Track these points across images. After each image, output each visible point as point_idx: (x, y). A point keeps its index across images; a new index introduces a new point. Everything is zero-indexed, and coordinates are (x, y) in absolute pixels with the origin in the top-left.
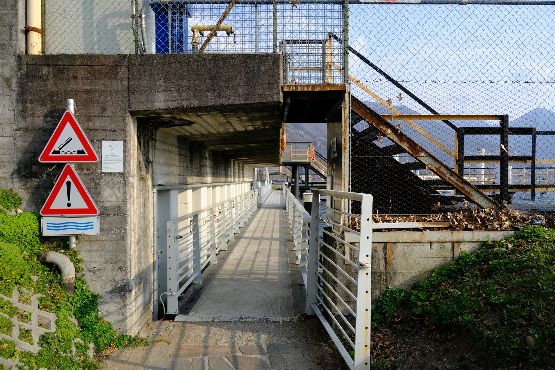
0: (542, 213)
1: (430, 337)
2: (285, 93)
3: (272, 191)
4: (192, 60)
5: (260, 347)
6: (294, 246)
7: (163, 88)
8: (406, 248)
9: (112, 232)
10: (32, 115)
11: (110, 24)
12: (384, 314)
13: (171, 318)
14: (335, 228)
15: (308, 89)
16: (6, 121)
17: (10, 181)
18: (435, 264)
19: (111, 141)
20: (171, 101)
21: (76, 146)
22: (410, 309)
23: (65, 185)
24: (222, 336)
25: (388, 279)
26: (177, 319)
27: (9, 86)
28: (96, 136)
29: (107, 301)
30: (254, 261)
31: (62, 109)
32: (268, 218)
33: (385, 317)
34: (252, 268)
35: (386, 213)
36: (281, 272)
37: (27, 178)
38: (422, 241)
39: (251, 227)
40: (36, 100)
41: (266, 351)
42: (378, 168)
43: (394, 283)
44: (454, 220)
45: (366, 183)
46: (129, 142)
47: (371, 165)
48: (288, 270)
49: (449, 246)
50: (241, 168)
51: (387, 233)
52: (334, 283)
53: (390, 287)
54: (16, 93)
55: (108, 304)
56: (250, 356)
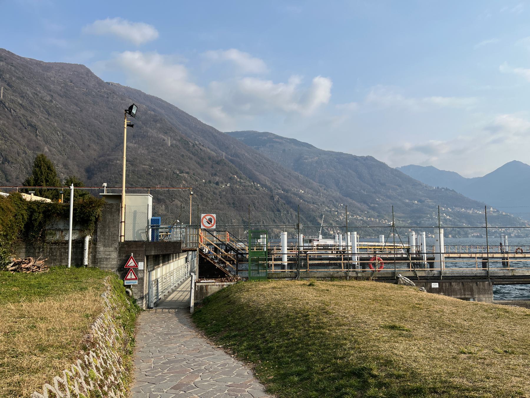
11: (139, 232)
13: (152, 308)
27: (117, 250)
39: (182, 287)
49: (221, 286)
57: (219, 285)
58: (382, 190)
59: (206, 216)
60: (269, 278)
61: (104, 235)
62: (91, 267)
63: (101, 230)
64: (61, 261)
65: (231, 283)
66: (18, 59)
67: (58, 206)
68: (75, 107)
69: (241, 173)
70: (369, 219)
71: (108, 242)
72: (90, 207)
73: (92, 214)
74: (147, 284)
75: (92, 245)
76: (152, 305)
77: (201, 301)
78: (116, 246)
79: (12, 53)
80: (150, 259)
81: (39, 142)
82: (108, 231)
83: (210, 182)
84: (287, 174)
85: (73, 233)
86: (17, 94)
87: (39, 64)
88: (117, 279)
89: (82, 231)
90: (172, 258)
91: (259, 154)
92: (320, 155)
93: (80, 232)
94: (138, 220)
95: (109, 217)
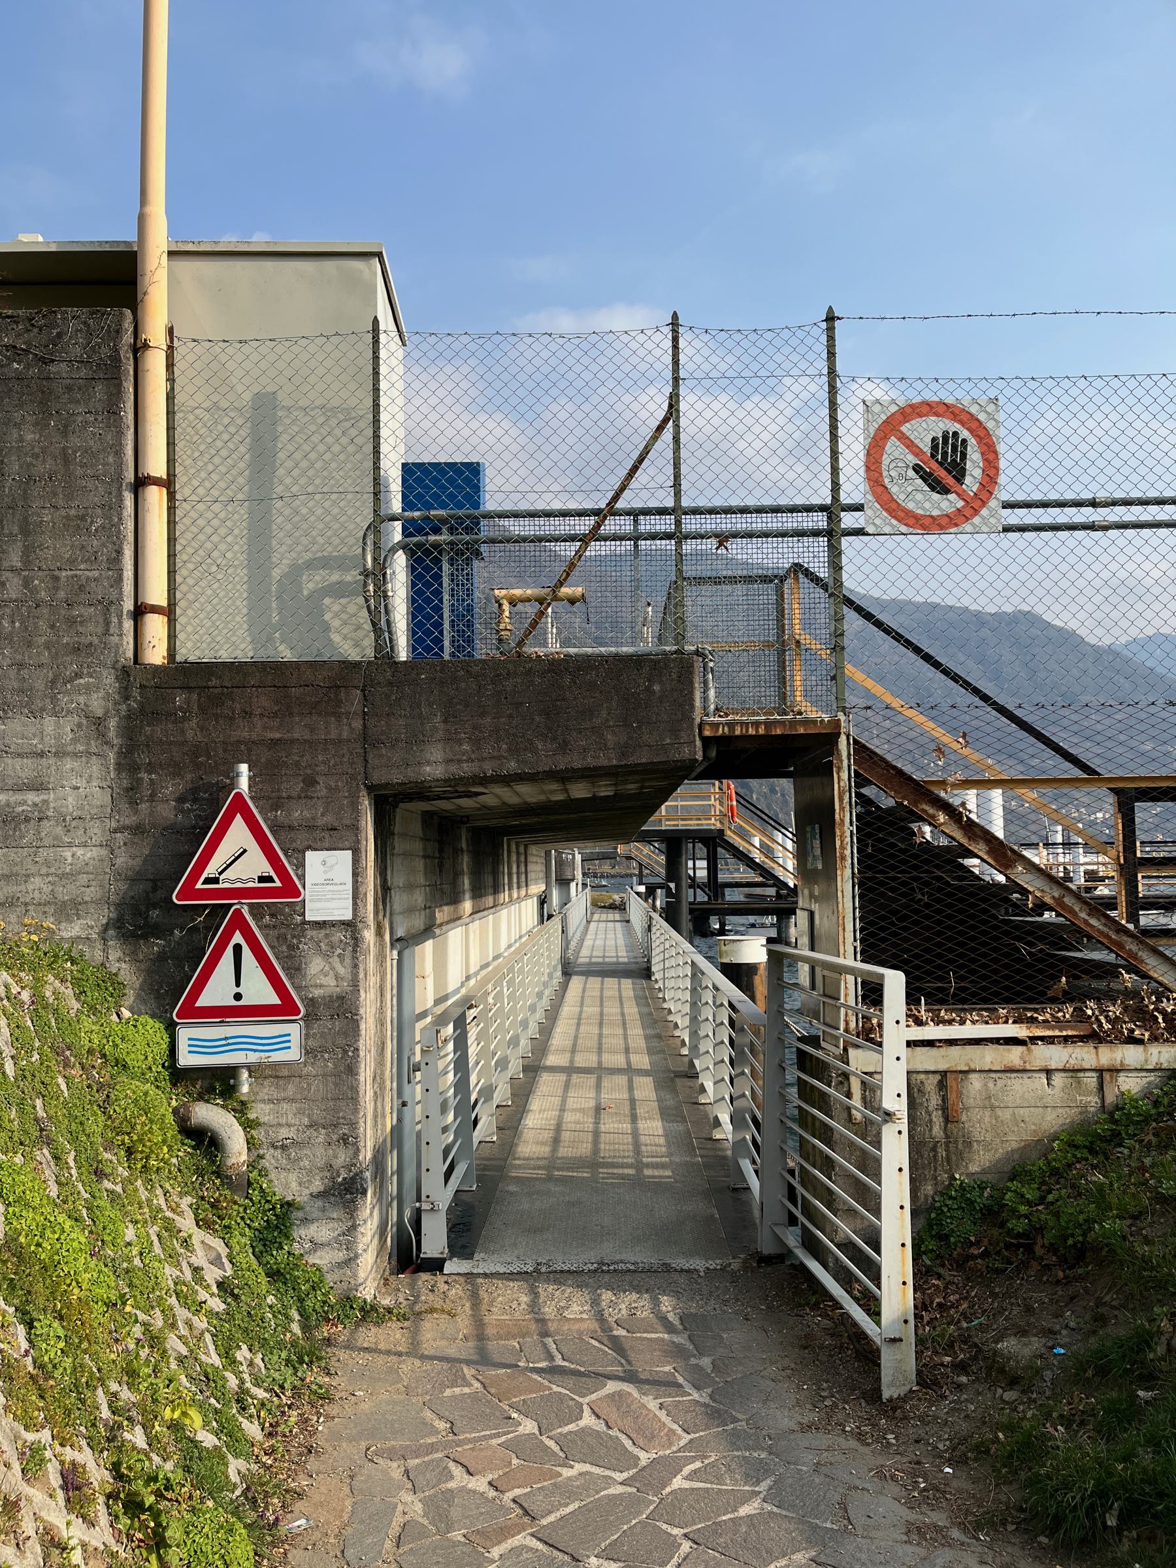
1: (1045, 1279)
2: (706, 741)
3: (592, 914)
4: (504, 673)
5: (663, 1319)
6: (703, 1090)
7: (440, 734)
8: (991, 1085)
9: (326, 1056)
12: (946, 1238)
13: (436, 1266)
14: (828, 1038)
15: (757, 731)
16: (94, 811)
17: (99, 945)
18: (1061, 1121)
19: (325, 852)
20: (460, 761)
21: (254, 866)
22: (1002, 1225)
24: (569, 1299)
25: (954, 1158)
26: (449, 1267)
28: (293, 840)
29: (314, 1216)
31: (217, 783)
32: (602, 1005)
33: (948, 1244)
34: (596, 1150)
35: (941, 1004)
36: (677, 1159)
37: (138, 937)
38: (1028, 1068)
39: (560, 1037)
40: (161, 765)
41: (681, 1327)
42: (921, 900)
43: (967, 1167)
44: (1102, 1018)
45: (894, 934)
46: (364, 853)
47: (904, 895)
48: (696, 1155)
49: (1091, 1080)
50: (522, 858)
51: (955, 1051)
52: (828, 1165)
53: (957, 1176)
54: (116, 749)
55: (316, 1224)
56: (645, 1335)
57: (1074, 1072)
71: (21, 665)
74: (389, 1047)
78: (97, 704)
82: (15, 560)
85: (847, 1236)
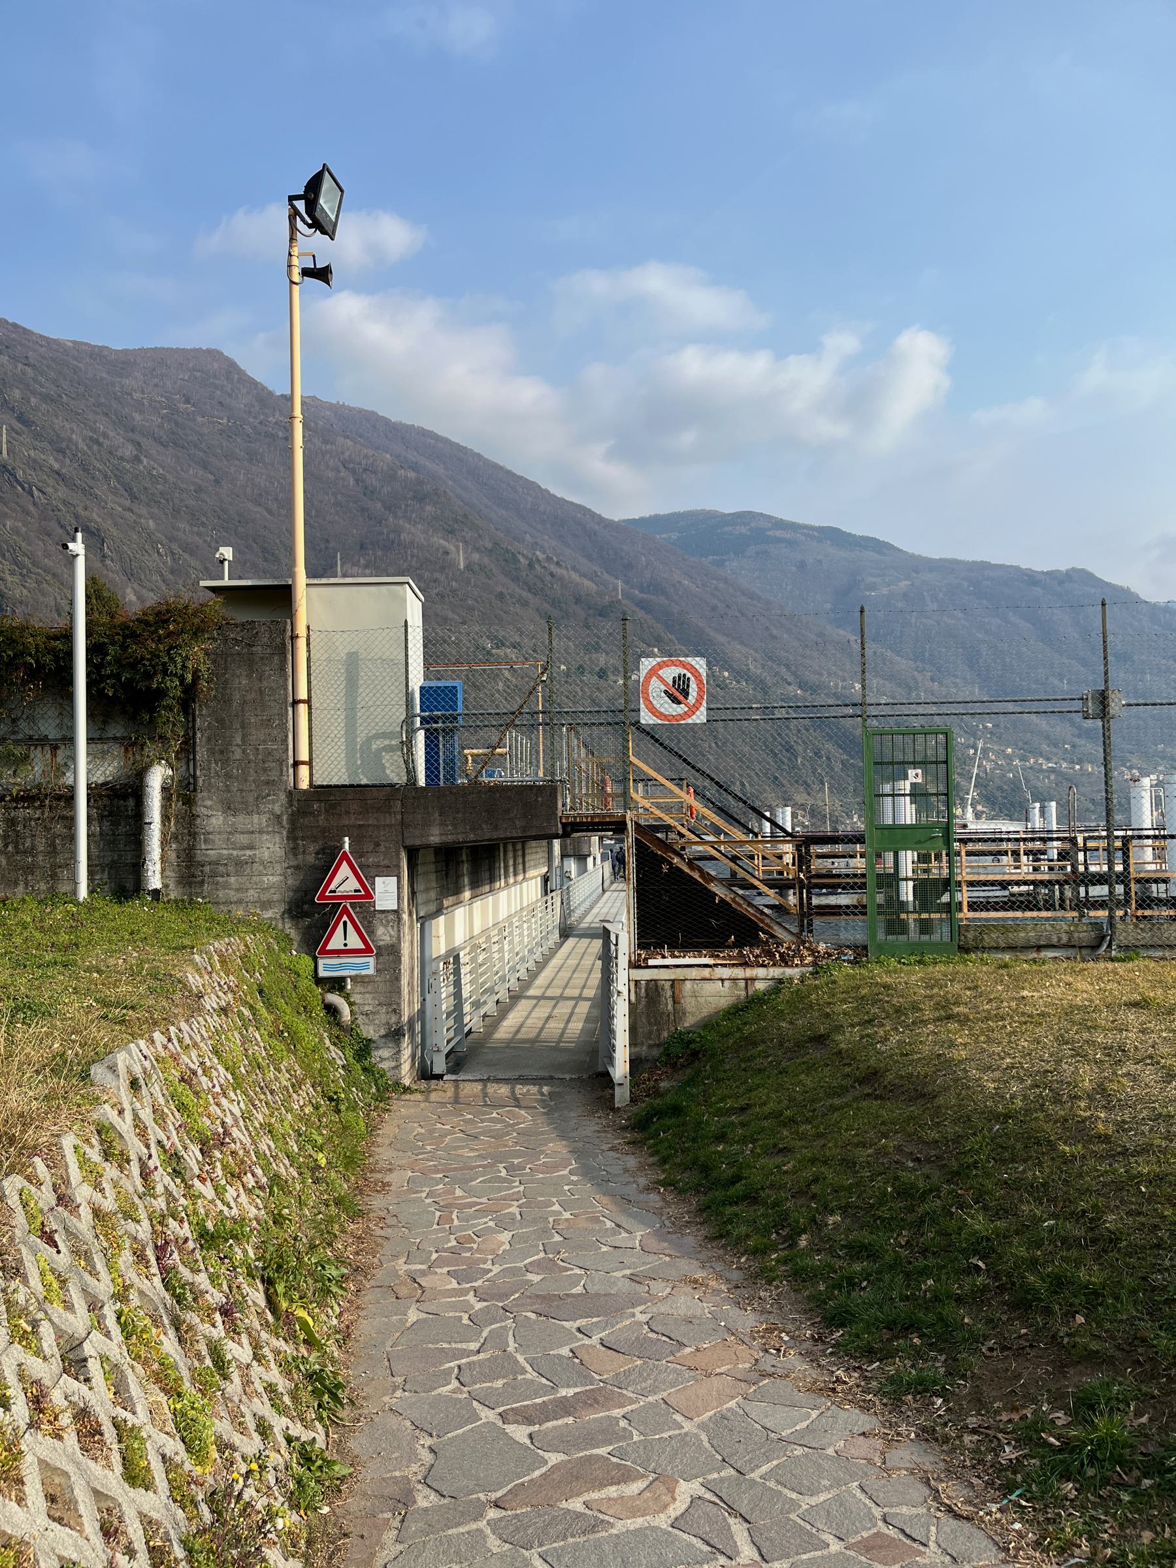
0: (848, 947)
10: (304, 852)
11: (374, 746)
13: (439, 1077)
21: (352, 885)
23: (341, 925)
26: (445, 1078)
27: (280, 823)
30: (542, 1029)
39: (542, 980)
49: (742, 984)
50: (520, 853)
57: (734, 980)
58: (1122, 675)
59: (660, 666)
60: (964, 949)
61: (226, 762)
62: (176, 901)
63: (209, 739)
64: (54, 876)
65: (789, 971)
66: (41, 346)
67: (26, 634)
68: (201, 472)
69: (671, 640)
70: (1078, 767)
72: (160, 636)
73: (164, 664)
74: (416, 971)
75: (177, 806)
76: (439, 1066)
77: (656, 1052)
78: (277, 809)
79: (24, 329)
80: (423, 864)
81: (111, 574)
82: (238, 740)
83: (581, 669)
84: (812, 636)
86: (45, 444)
87: (98, 354)
88: (283, 950)
89: (133, 744)
90: (502, 872)
91: (726, 581)
92: (917, 572)
93: (126, 750)
94: (364, 695)
95: (241, 681)
